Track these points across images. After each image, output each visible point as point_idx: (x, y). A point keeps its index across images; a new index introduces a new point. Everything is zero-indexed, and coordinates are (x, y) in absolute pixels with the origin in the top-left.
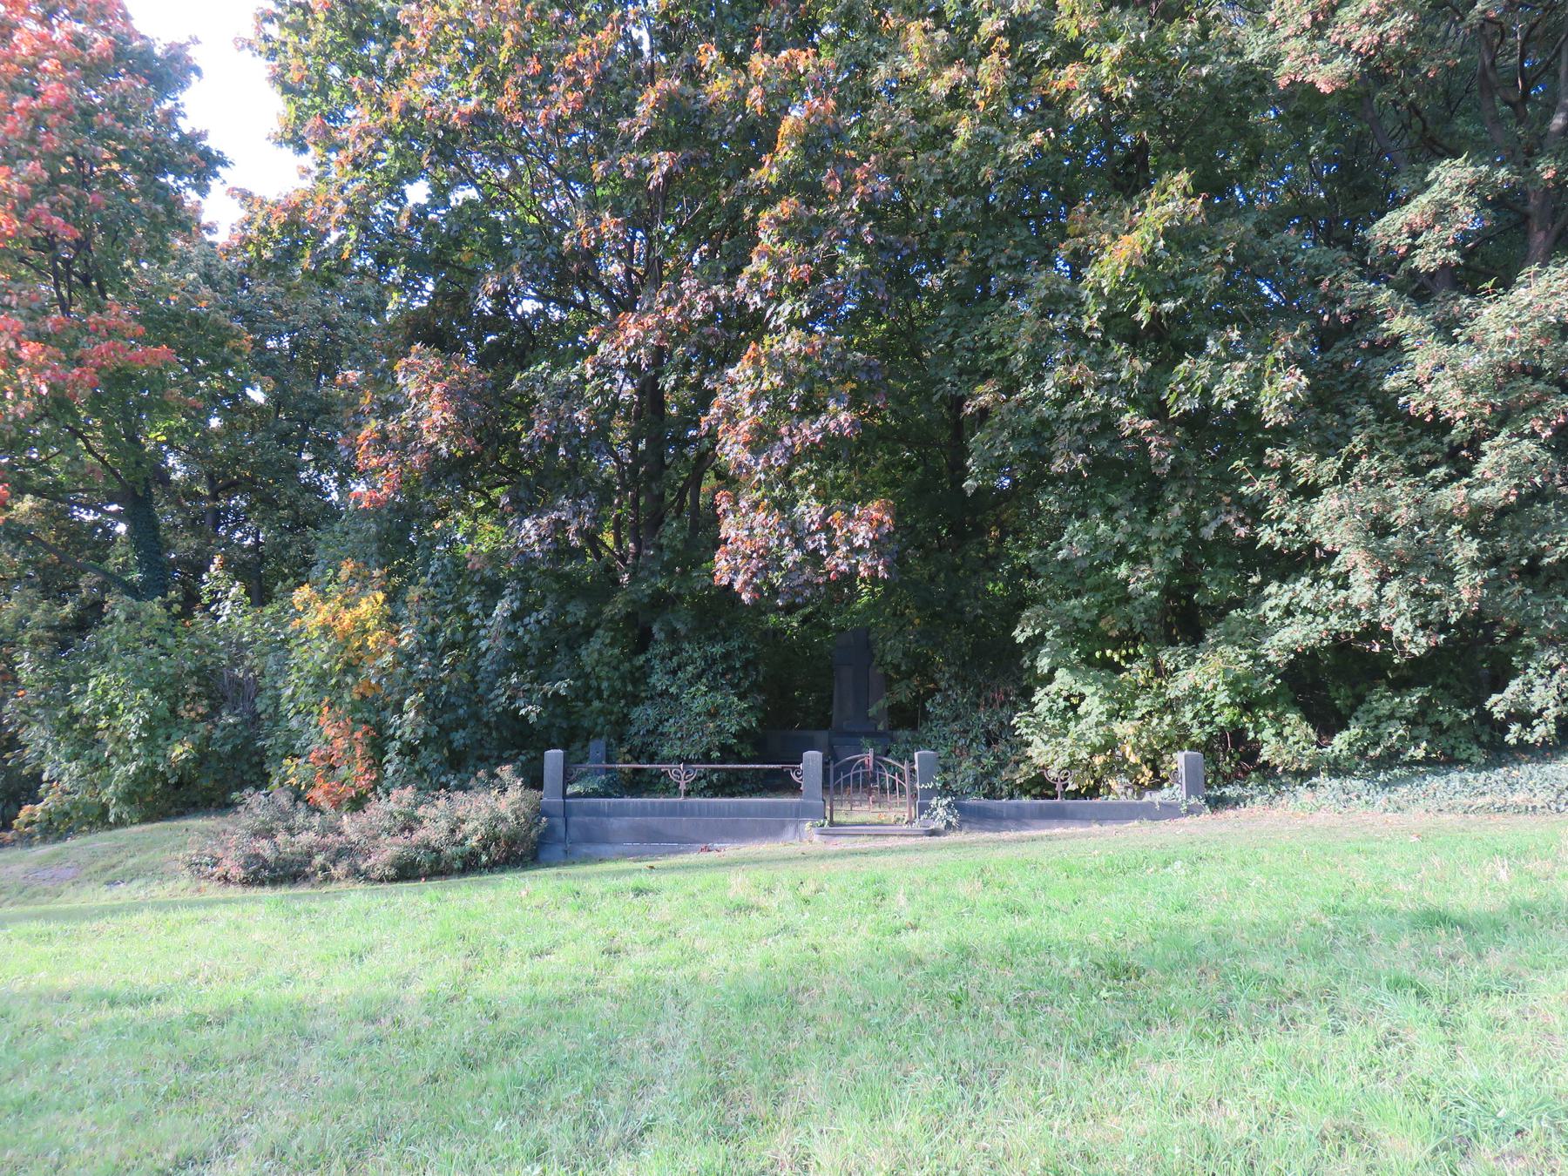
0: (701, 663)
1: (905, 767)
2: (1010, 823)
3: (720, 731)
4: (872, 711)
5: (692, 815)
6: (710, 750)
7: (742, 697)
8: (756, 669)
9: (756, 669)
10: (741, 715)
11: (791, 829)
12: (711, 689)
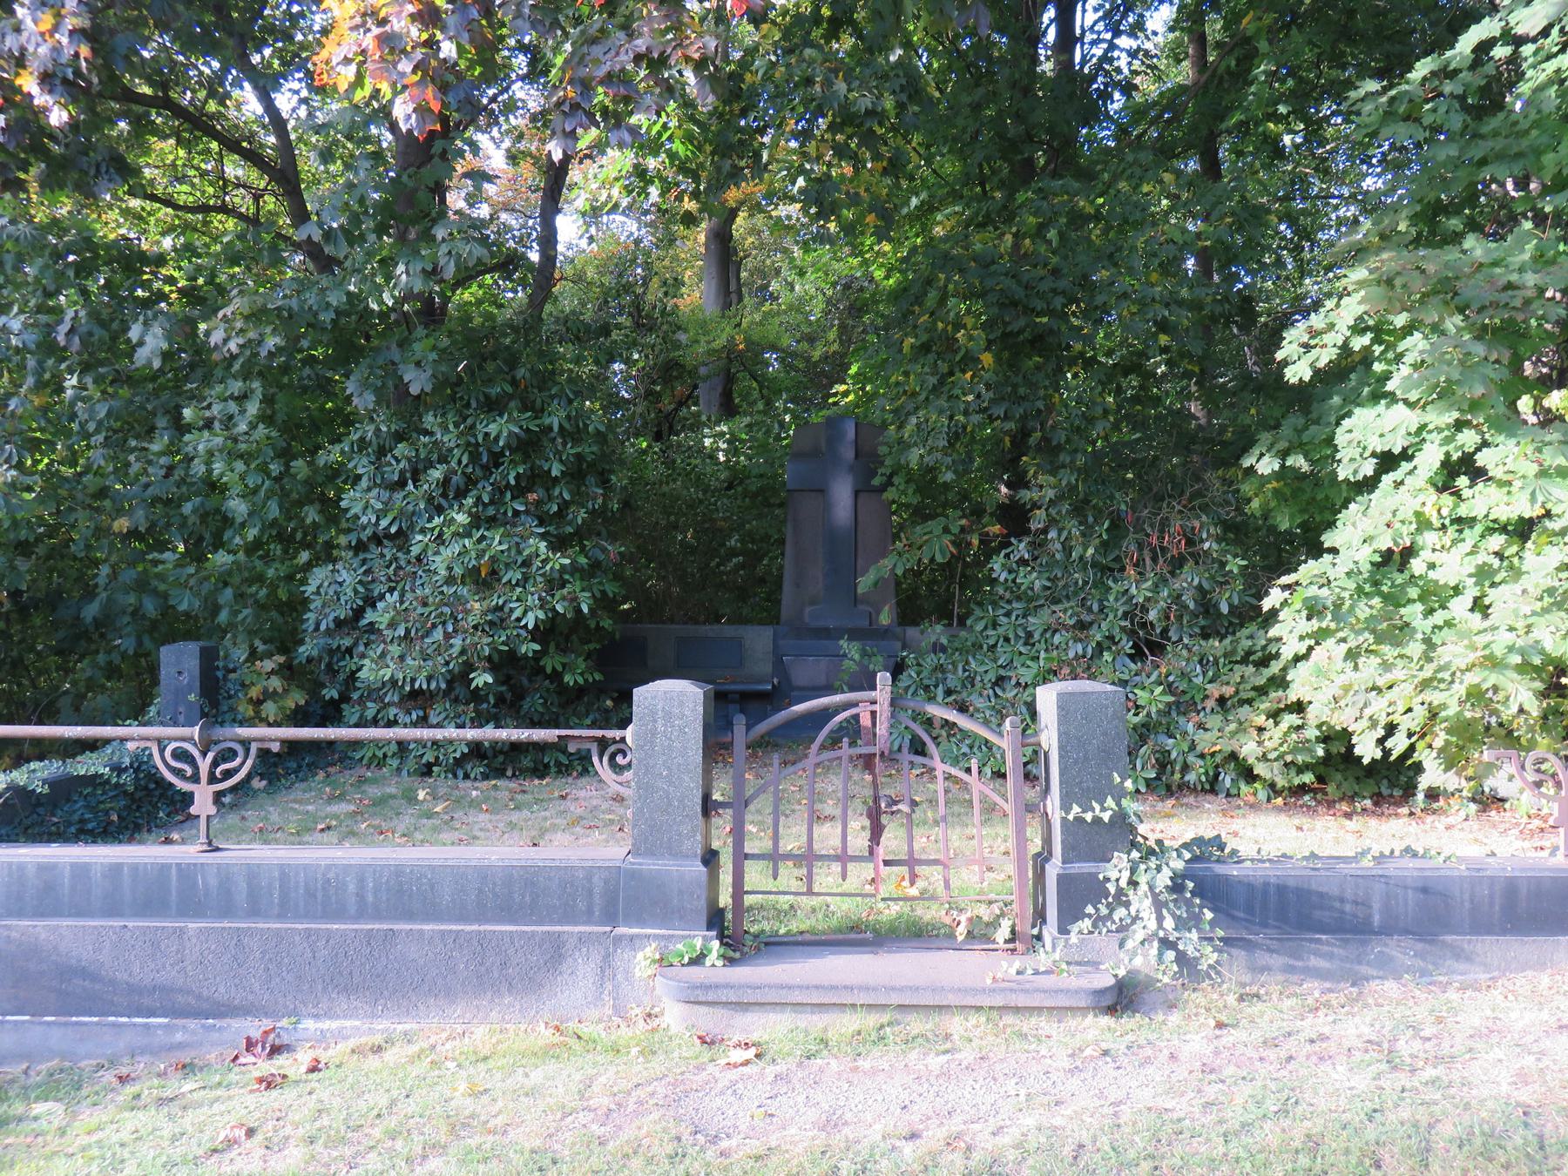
0: (460, 458)
1: (1006, 741)
2: (1399, 949)
3: (497, 620)
4: (865, 583)
5: (226, 909)
6: (469, 667)
7: (559, 544)
8: (604, 482)
9: (604, 482)
10: (555, 583)
11: (583, 969)
12: (476, 521)
